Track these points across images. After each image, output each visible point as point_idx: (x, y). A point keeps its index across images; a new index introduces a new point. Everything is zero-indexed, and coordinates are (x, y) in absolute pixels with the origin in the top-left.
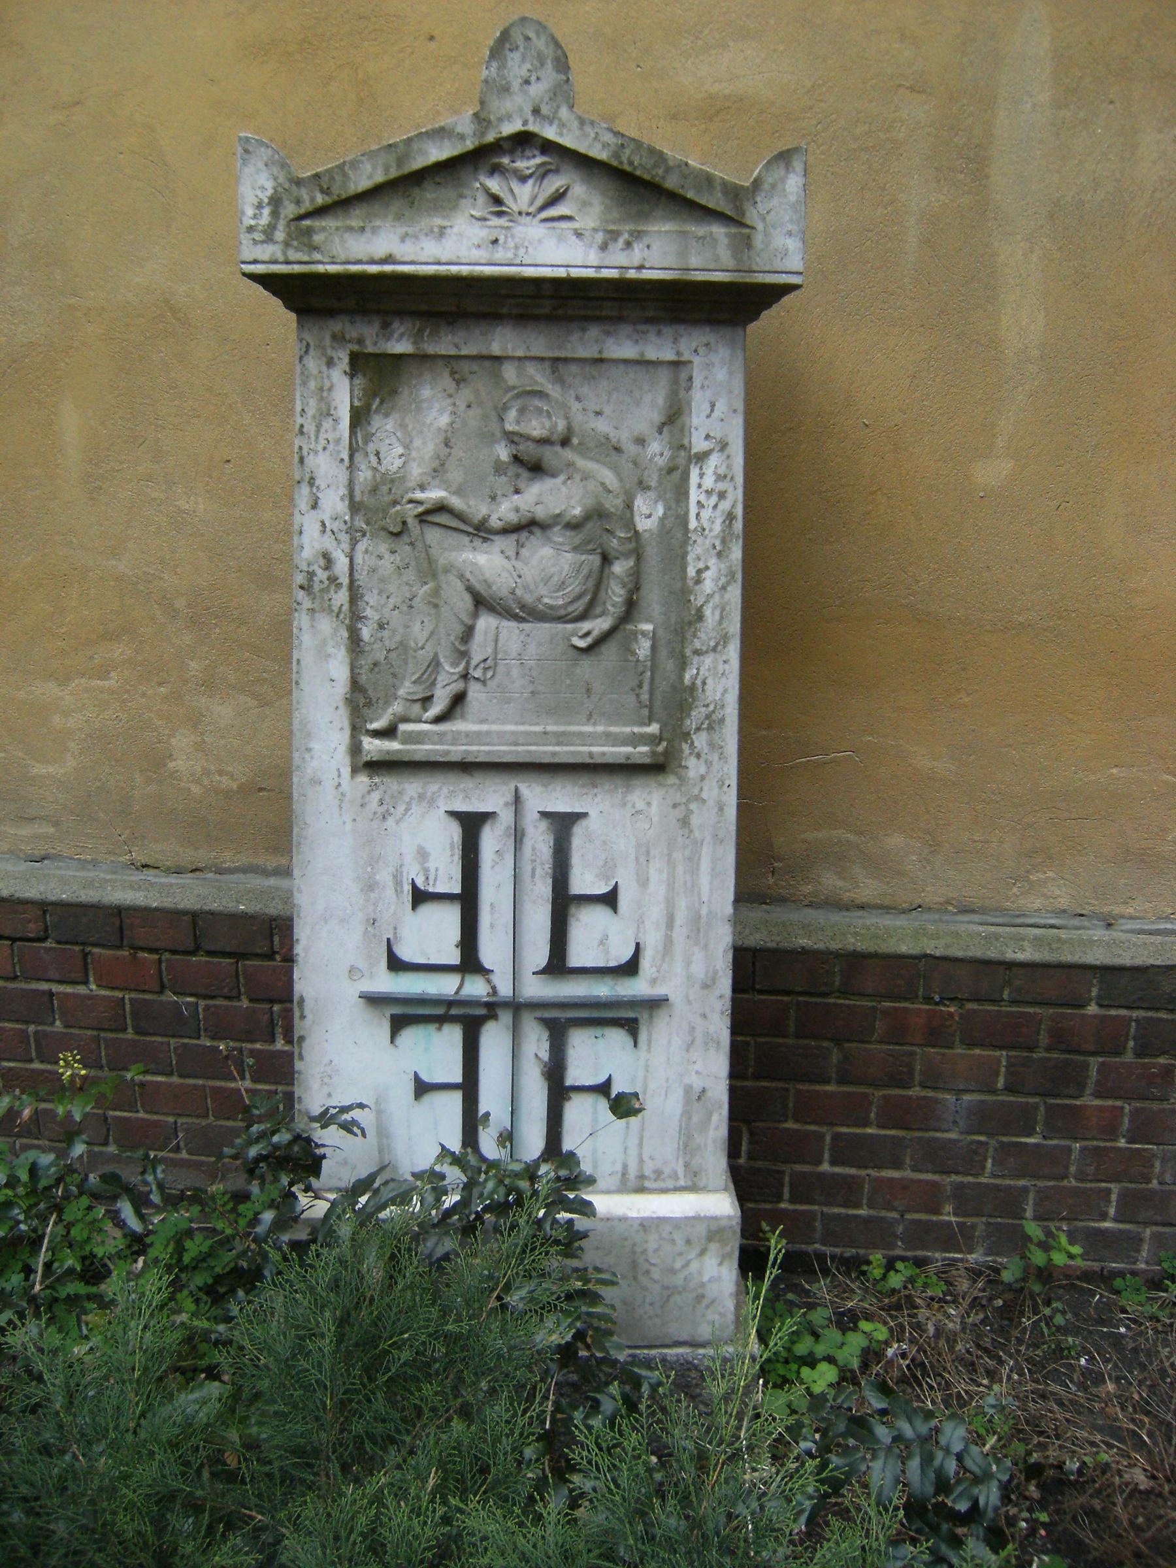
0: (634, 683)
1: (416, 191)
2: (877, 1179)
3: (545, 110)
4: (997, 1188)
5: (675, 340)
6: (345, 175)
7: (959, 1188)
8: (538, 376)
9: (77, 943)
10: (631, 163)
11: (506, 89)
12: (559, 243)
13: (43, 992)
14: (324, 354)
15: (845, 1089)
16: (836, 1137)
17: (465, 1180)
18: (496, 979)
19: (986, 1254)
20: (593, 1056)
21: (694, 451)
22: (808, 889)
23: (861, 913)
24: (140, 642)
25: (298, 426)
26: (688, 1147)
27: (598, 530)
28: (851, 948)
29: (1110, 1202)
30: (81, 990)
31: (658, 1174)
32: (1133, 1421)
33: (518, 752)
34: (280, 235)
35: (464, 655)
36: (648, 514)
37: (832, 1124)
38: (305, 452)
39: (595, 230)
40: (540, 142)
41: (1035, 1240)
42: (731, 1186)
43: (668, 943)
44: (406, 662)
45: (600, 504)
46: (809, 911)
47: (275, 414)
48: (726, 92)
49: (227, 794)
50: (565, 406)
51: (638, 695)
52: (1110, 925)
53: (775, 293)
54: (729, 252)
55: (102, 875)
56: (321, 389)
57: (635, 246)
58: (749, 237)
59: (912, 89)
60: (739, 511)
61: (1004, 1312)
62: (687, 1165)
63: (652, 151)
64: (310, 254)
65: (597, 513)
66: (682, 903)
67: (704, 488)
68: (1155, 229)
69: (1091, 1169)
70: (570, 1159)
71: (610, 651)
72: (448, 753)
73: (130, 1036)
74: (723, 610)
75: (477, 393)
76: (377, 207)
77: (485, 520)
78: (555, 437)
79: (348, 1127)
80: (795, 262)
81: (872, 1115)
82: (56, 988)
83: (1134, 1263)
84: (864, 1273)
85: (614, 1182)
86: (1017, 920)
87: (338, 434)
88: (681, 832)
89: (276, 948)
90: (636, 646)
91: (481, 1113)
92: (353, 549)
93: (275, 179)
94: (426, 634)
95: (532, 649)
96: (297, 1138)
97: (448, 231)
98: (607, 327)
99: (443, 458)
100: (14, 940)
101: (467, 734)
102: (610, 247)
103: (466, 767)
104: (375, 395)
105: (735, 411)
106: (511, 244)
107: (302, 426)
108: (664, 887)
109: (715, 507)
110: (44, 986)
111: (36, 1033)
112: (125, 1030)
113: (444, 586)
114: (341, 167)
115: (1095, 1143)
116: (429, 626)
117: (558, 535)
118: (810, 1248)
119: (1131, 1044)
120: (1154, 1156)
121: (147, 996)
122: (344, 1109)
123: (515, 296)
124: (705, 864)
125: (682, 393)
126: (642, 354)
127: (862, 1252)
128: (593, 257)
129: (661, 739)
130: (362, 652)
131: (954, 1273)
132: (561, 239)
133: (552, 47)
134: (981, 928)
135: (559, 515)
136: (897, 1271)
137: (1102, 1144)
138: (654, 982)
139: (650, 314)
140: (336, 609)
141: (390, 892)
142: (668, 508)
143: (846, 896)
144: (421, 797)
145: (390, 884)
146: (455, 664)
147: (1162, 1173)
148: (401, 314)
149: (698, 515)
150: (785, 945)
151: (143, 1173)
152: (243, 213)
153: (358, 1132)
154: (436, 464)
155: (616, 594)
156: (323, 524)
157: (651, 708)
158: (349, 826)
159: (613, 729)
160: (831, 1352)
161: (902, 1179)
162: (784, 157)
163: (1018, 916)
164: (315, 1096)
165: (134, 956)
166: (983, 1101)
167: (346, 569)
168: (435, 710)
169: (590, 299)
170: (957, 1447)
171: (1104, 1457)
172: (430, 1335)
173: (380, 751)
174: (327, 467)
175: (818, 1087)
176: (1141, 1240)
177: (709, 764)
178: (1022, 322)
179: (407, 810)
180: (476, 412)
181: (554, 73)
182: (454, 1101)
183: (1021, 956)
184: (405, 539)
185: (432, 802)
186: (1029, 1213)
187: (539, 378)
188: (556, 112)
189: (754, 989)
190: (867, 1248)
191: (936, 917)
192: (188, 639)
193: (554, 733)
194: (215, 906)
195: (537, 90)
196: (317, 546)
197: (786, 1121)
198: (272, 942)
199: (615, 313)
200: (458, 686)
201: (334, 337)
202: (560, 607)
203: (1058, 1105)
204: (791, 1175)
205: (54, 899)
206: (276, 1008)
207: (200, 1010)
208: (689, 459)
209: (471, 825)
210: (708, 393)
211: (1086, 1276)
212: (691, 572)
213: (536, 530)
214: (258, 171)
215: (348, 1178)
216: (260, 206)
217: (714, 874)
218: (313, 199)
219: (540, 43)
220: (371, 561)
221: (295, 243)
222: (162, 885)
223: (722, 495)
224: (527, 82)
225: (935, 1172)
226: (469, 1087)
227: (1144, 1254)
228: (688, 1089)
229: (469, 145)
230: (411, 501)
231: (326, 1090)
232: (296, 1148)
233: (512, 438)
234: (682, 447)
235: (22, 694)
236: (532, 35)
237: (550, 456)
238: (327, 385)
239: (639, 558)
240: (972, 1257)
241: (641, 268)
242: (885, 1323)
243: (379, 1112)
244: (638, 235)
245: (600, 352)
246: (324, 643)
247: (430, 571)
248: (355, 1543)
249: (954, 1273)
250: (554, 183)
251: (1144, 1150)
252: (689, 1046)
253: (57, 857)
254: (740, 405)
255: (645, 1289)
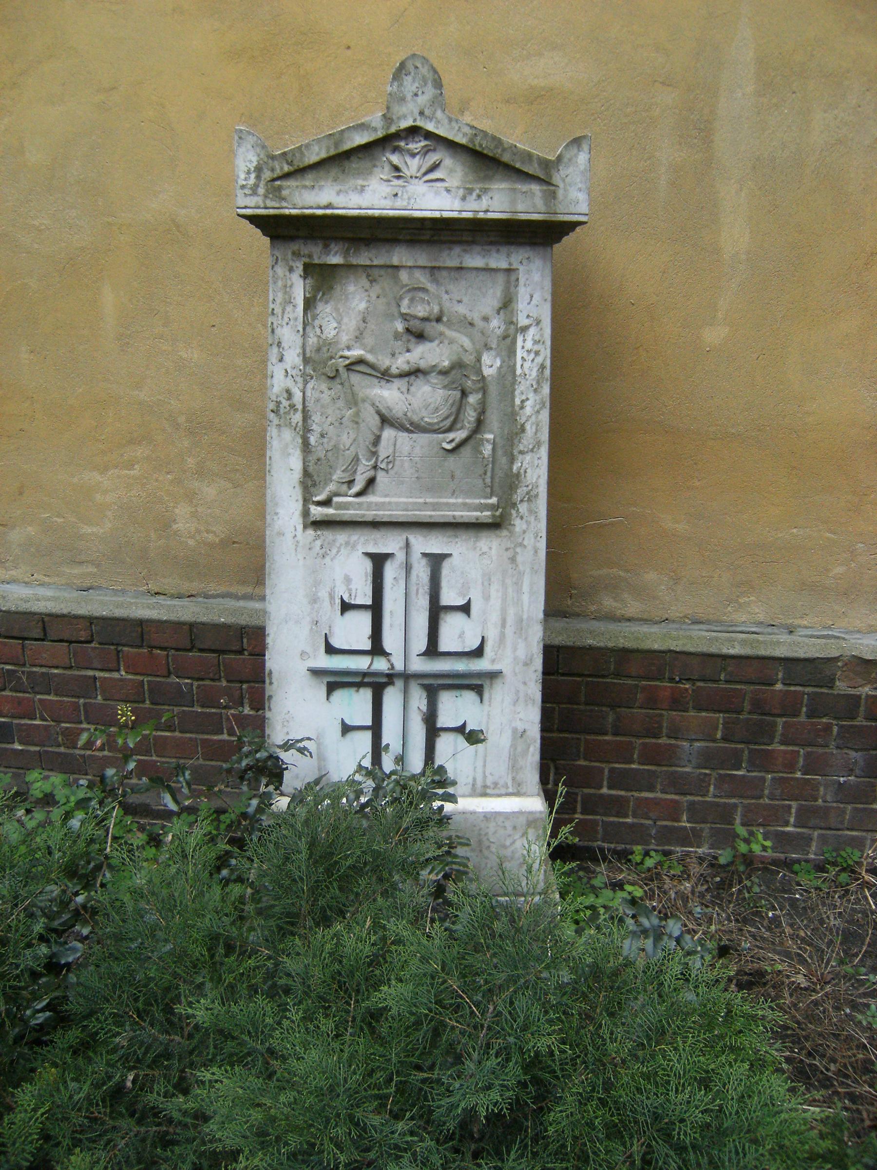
0: (481, 472)
1: (346, 163)
2: (637, 799)
3: (427, 112)
4: (717, 805)
5: (508, 256)
6: (302, 153)
7: (692, 804)
8: (422, 278)
9: (113, 644)
10: (481, 145)
11: (403, 99)
12: (435, 194)
13: (90, 677)
14: (287, 264)
15: (618, 738)
16: (612, 770)
17: (374, 786)
18: (393, 659)
19: (710, 849)
20: (454, 708)
21: (519, 326)
22: (593, 608)
23: (628, 624)
24: (155, 445)
25: (270, 310)
26: (514, 767)
27: (459, 375)
28: (621, 646)
29: (790, 813)
30: (116, 675)
31: (496, 784)
32: (800, 948)
33: (409, 515)
34: (261, 191)
35: (374, 454)
36: (491, 365)
37: (608, 762)
38: (275, 326)
39: (458, 188)
40: (423, 133)
41: (742, 837)
42: (542, 794)
43: (502, 637)
44: (337, 458)
45: (460, 359)
46: (594, 622)
47: (245, 295)
48: (542, 85)
49: (212, 545)
50: (439, 297)
51: (484, 480)
52: (791, 632)
53: (571, 226)
54: (542, 202)
55: (128, 600)
56: (285, 286)
57: (483, 197)
58: (554, 193)
59: (663, 83)
60: (548, 363)
61: (721, 886)
62: (514, 779)
63: (494, 138)
64: (280, 202)
65: (458, 365)
66: (511, 612)
67: (526, 348)
68: (822, 176)
69: (778, 792)
70: (441, 769)
71: (466, 451)
72: (364, 515)
73: (147, 706)
74: (537, 425)
75: (383, 289)
76: (322, 173)
77: (388, 369)
78: (432, 317)
79: (302, 751)
80: (584, 208)
81: (635, 756)
82: (98, 674)
83: (807, 854)
84: (629, 860)
85: (468, 789)
86: (730, 628)
87: (296, 315)
88: (510, 566)
89: (245, 646)
90: (482, 448)
91: (384, 744)
92: (305, 387)
93: (259, 155)
94: (350, 441)
95: (417, 451)
96: (271, 757)
97: (367, 188)
98: (465, 247)
99: (362, 329)
100: (71, 642)
101: (376, 504)
102: (467, 198)
103: (375, 525)
104: (319, 290)
105: (546, 300)
106: (405, 196)
107: (273, 309)
108: (499, 598)
109: (533, 360)
110: (90, 673)
111: (85, 704)
112: (144, 702)
113: (362, 410)
114: (300, 148)
115: (781, 775)
116: (353, 435)
117: (434, 378)
118: (595, 844)
119: (804, 709)
120: (819, 783)
121: (158, 679)
122: (298, 741)
123: (408, 229)
124: (526, 588)
125: (512, 289)
126: (487, 264)
127: (628, 847)
128: (457, 204)
129: (498, 507)
130: (310, 452)
131: (688, 860)
132: (437, 193)
133: (431, 73)
134: (707, 634)
135: (434, 366)
136: (651, 857)
137: (785, 775)
138: (493, 661)
139: (493, 239)
140: (294, 425)
141: (327, 603)
142: (503, 362)
143: (618, 613)
144: (347, 543)
145: (327, 599)
146: (368, 460)
147: (825, 795)
148: (336, 239)
149: (522, 365)
150: (578, 644)
151: (177, 776)
152: (238, 177)
153: (308, 754)
154: (357, 333)
155: (470, 416)
156: (286, 371)
157: (492, 487)
158: (301, 562)
159: (467, 501)
160: (606, 903)
161: (655, 798)
162: (577, 142)
163: (732, 626)
164: (277, 735)
165: (151, 652)
166: (707, 747)
167: (301, 400)
168: (356, 488)
169: (456, 230)
170: (676, 933)
171: (780, 967)
172: (363, 852)
173: (322, 514)
174: (289, 336)
175: (600, 738)
176: (811, 839)
177: (528, 523)
178: (735, 236)
179: (338, 552)
180: (383, 300)
181: (433, 90)
182: (366, 738)
183: (732, 652)
184: (338, 380)
185: (354, 547)
186: (738, 821)
187: (422, 279)
188: (434, 113)
189: (558, 673)
190: (631, 844)
191: (677, 626)
192: (186, 443)
193: (431, 503)
194: (204, 619)
195: (422, 100)
196: (283, 385)
197: (579, 759)
198: (242, 643)
199: (470, 239)
200: (371, 473)
201: (294, 253)
202: (436, 423)
203: (756, 749)
204: (582, 796)
205: (97, 615)
206: (245, 686)
207: (194, 688)
208: (517, 330)
209: (379, 561)
210: (529, 289)
211: (775, 862)
212: (518, 402)
213: (420, 375)
214: (248, 151)
215: (299, 785)
216: (249, 173)
217: (532, 593)
218: (282, 168)
219: (424, 70)
220: (317, 395)
221: (271, 196)
222: (169, 606)
223: (537, 353)
224: (416, 95)
225: (676, 794)
226: (376, 728)
227: (813, 848)
228: (515, 730)
229: (380, 134)
230: (341, 357)
231: (285, 730)
232: (269, 763)
233: (405, 317)
234: (512, 323)
235: (75, 480)
236: (419, 65)
237: (430, 328)
238: (289, 283)
239: (484, 393)
240: (700, 851)
241: (487, 211)
242: (641, 887)
243: (319, 745)
244: (485, 191)
245: (461, 263)
246: (287, 446)
247: (353, 401)
248: (325, 958)
249: (688, 860)
250: (433, 158)
251: (813, 779)
252: (516, 702)
253: (99, 588)
254: (549, 298)
255: (487, 858)
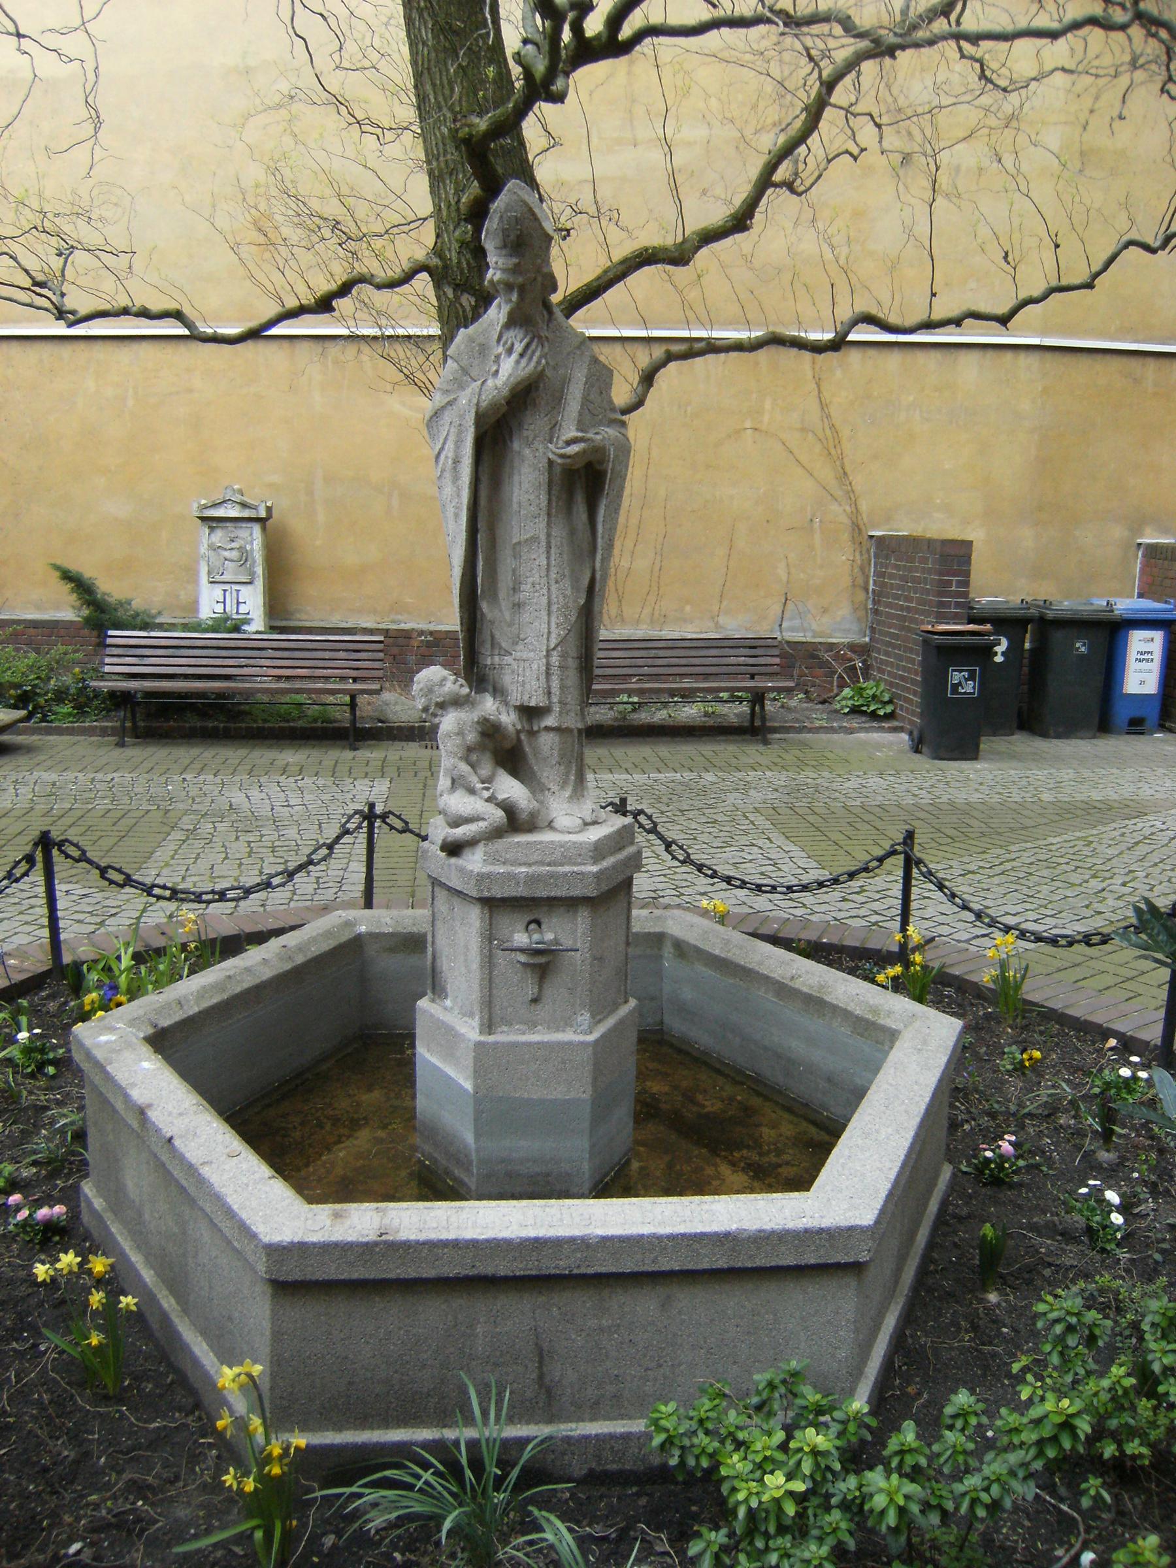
12: (234, 512)
27: (241, 549)
174: (205, 541)
209: (225, 591)
